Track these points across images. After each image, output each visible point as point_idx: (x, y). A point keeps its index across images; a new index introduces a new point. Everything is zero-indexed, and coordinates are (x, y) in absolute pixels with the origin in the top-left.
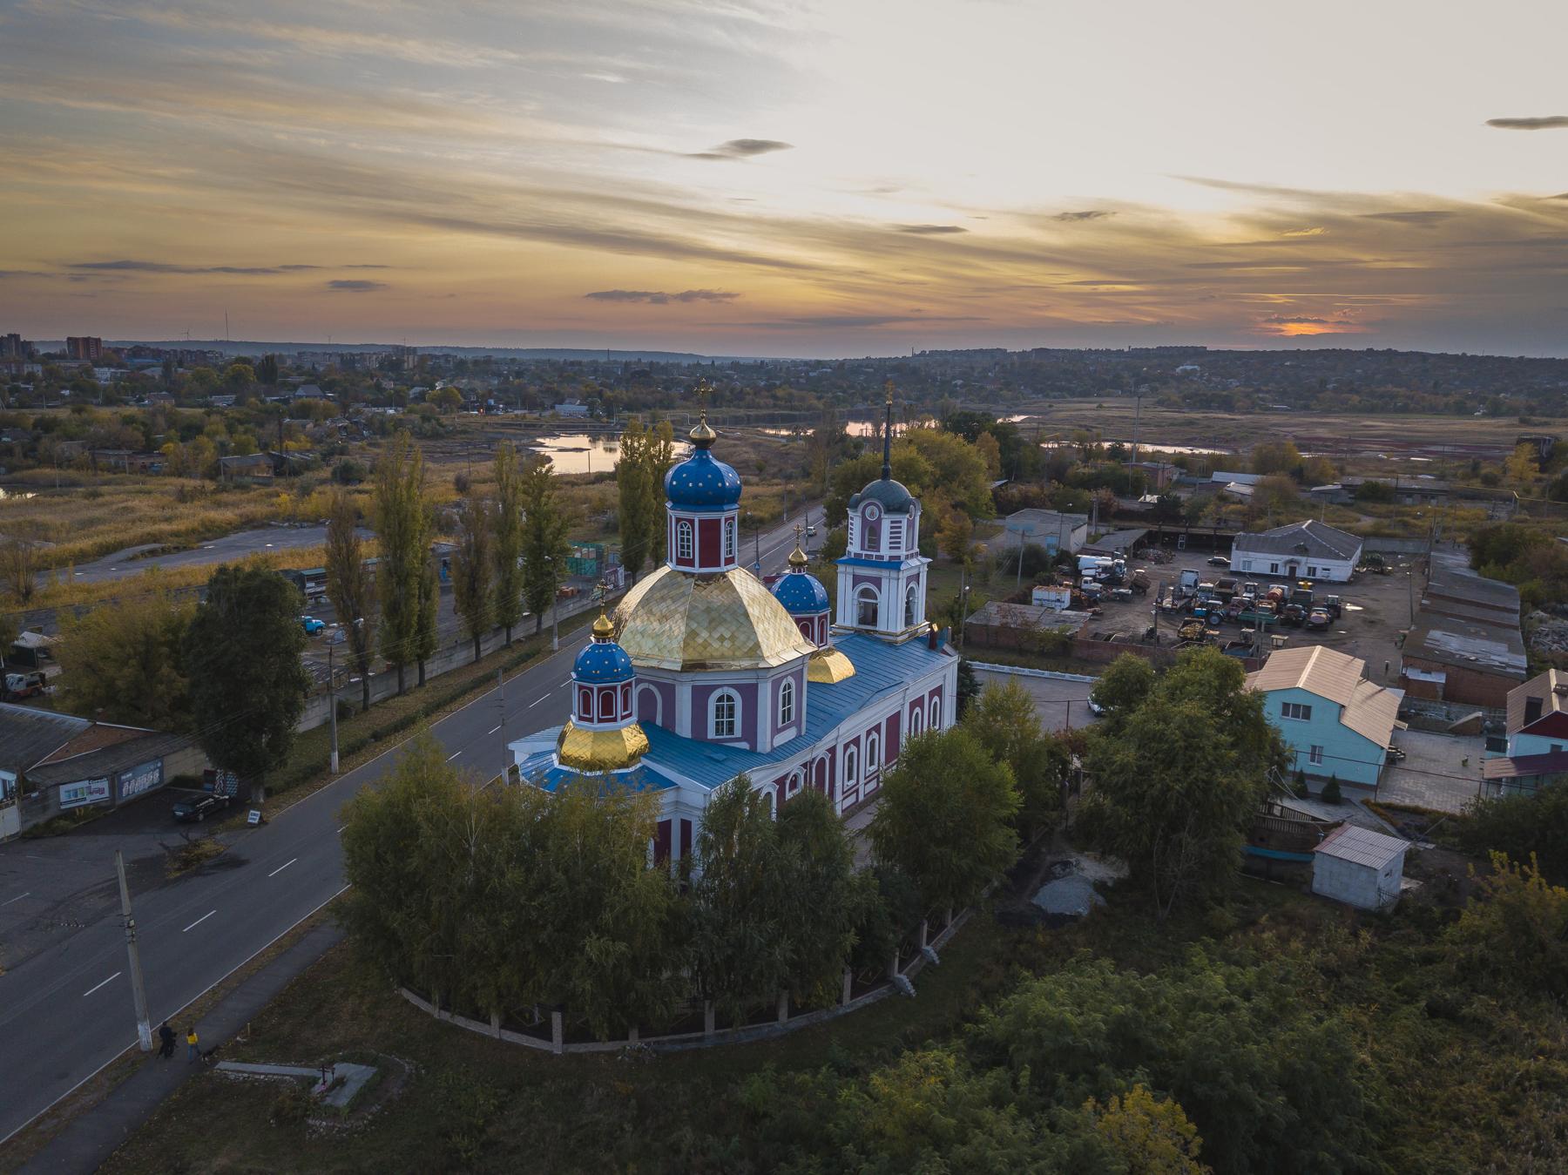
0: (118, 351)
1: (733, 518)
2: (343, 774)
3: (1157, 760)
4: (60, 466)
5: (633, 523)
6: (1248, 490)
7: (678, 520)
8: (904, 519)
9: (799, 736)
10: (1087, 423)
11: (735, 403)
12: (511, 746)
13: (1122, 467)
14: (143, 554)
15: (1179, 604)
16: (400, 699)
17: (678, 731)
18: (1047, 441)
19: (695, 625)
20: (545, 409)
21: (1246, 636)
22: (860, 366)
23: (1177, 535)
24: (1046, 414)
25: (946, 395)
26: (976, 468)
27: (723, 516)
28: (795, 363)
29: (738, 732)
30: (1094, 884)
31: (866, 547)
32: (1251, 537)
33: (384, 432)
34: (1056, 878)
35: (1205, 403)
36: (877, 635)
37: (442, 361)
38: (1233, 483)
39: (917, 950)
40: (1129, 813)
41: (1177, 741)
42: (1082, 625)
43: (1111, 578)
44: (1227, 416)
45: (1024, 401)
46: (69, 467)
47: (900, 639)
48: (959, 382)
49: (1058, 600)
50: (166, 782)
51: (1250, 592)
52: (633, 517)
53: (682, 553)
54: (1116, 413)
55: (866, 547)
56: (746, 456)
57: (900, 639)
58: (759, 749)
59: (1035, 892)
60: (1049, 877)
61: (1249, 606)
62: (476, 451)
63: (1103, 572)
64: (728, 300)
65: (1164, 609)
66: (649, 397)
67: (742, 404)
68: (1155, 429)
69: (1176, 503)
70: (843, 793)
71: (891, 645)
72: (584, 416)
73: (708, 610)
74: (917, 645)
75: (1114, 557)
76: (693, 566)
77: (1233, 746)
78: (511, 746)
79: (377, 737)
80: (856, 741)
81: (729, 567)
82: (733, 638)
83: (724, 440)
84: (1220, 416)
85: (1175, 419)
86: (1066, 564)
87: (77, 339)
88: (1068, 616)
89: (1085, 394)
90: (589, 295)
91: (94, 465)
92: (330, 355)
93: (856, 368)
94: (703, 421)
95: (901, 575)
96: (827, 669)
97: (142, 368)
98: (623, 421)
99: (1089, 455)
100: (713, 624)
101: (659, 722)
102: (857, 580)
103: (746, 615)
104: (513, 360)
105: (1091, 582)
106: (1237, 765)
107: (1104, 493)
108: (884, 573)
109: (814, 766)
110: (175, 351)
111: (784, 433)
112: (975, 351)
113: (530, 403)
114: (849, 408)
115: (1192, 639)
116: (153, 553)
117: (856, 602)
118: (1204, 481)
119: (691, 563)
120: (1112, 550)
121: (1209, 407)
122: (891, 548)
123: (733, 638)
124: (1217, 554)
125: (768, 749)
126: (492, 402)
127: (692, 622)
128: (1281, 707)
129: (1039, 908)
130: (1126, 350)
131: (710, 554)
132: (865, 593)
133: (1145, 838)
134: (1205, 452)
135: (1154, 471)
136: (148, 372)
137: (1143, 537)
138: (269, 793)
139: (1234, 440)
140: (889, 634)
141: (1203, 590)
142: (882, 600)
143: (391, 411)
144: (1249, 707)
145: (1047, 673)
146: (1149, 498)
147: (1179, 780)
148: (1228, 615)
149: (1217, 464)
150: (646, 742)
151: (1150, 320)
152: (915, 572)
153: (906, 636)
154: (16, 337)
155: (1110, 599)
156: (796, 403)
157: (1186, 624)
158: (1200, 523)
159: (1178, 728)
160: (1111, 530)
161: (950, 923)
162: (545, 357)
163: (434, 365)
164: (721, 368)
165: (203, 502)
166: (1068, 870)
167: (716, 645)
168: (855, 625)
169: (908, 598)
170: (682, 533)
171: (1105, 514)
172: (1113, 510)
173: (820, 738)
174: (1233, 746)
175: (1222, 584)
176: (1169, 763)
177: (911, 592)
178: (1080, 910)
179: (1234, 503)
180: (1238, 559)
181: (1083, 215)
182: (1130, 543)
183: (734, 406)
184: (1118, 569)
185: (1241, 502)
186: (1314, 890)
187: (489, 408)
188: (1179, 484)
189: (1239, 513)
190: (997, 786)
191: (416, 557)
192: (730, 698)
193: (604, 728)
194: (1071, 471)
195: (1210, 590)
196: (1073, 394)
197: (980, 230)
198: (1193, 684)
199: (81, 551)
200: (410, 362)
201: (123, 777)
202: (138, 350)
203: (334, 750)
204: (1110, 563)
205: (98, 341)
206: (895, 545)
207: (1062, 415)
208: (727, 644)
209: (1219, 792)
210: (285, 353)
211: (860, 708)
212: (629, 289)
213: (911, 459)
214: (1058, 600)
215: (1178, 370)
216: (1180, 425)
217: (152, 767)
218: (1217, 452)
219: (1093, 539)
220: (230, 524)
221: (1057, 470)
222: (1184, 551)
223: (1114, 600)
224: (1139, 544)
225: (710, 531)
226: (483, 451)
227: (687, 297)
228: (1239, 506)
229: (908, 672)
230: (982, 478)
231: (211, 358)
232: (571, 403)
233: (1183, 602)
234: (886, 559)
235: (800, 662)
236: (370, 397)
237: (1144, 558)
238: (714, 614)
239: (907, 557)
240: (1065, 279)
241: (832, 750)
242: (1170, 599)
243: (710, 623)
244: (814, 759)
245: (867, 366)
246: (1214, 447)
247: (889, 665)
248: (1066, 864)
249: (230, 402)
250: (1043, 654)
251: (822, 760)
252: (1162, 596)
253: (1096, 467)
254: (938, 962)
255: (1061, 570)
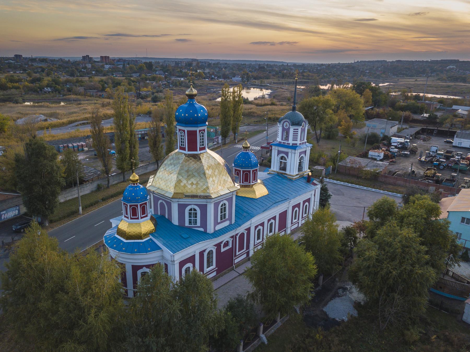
0: (114, 60)
1: (204, 130)
2: (83, 214)
3: (387, 255)
4: (76, 95)
5: (225, 120)
6: (466, 113)
7: (180, 130)
8: (300, 129)
9: (231, 224)
10: (409, 86)
11: (290, 77)
12: (111, 221)
13: (417, 103)
14: (81, 124)
15: (428, 159)
16: (123, 183)
17: (173, 222)
18: (392, 92)
19: (181, 177)
20: (229, 79)
21: (453, 177)
22: (335, 66)
23: (434, 130)
24: (396, 82)
25: (362, 76)
26: (359, 102)
27: (198, 129)
28: (315, 65)
29: (199, 224)
30: (355, 303)
31: (284, 139)
32: (463, 133)
33: (176, 86)
34: (339, 297)
35: (456, 79)
36: (286, 175)
37: (204, 63)
38: (460, 110)
39: (257, 336)
40: (370, 280)
41: (398, 249)
42: (384, 168)
43: (403, 147)
44: (464, 84)
45: (390, 78)
46: (79, 95)
47: (294, 177)
48: (368, 71)
49: (378, 156)
50: (21, 214)
51: (459, 156)
52: (225, 118)
53: (182, 145)
54: (421, 83)
55: (284, 139)
56: (287, 95)
57: (294, 177)
58: (208, 231)
59: (326, 304)
60: (336, 295)
61: (457, 163)
62: (202, 92)
63: (400, 144)
64: (294, 44)
65: (421, 161)
66: (262, 75)
67: (292, 77)
68: (435, 89)
69: (436, 117)
70: (254, 245)
71: (291, 180)
72: (241, 81)
73: (187, 171)
74: (303, 180)
75: (406, 138)
76: (185, 150)
77: (427, 253)
78: (111, 221)
79: (104, 200)
80: (262, 224)
81: (202, 152)
82: (197, 183)
83: (281, 90)
84: (460, 84)
85: (443, 85)
86: (387, 140)
87: (103, 57)
88: (379, 164)
89: (412, 76)
90: (251, 43)
91: (85, 95)
92: (173, 61)
93: (334, 66)
94: (191, 86)
95: (296, 152)
96: (254, 192)
97: (118, 65)
98: (251, 83)
99: (407, 98)
100: (189, 177)
101: (175, 221)
102: (279, 152)
103: (204, 174)
104: (226, 63)
105: (394, 148)
106: (427, 263)
107: (407, 113)
108: (289, 150)
109: (238, 237)
110: (129, 60)
111: (302, 87)
112: (376, 61)
113: (225, 77)
114: (328, 80)
115: (429, 176)
116: (84, 124)
117: (278, 161)
118: (449, 108)
119: (184, 149)
120: (405, 135)
121: (457, 81)
122: (293, 140)
123: (197, 183)
124: (449, 138)
125: (212, 231)
126: (213, 76)
127: (180, 176)
128: (461, 219)
129: (325, 314)
130: (429, 61)
131: (192, 145)
132: (282, 158)
133: (376, 293)
134: (452, 97)
135: (429, 105)
136: (119, 66)
137: (420, 130)
138: (51, 222)
139: (464, 93)
140: (290, 175)
141: (439, 154)
142: (288, 161)
143: (182, 79)
144: (441, 228)
145: (365, 188)
146: (425, 115)
147: (396, 269)
148: (448, 165)
149: (455, 102)
150: (154, 228)
151: (439, 50)
152: (304, 150)
153: (298, 176)
154: (88, 56)
155: (400, 156)
156: (310, 78)
157: (428, 169)
158: (444, 126)
159: (400, 242)
160: (408, 127)
161: (279, 320)
162: (236, 62)
163: (202, 64)
164: (290, 66)
165: (109, 107)
166: (345, 293)
167: (189, 187)
168: (278, 171)
169: (300, 160)
170: (181, 136)
171: (407, 120)
172: (411, 119)
173: (240, 226)
174: (427, 253)
175: (448, 152)
176: (393, 259)
177: (301, 159)
178: (344, 318)
179: (459, 117)
180: (456, 141)
181: (418, 14)
182: (414, 133)
183: (289, 78)
184: (406, 143)
185: (462, 117)
186: (463, 320)
187: (212, 78)
188: (439, 110)
189: (461, 121)
190: (304, 265)
191: (128, 134)
192: (195, 210)
193: (133, 222)
194: (397, 104)
195: (442, 155)
196: (407, 75)
197: (382, 19)
198: (413, 216)
199: (63, 122)
200: (194, 64)
201: (2, 213)
202: (120, 60)
203: (80, 206)
204: (403, 141)
205: (108, 57)
206: (295, 139)
207: (402, 83)
208: (194, 186)
209: (416, 277)
210: (160, 61)
211: (263, 211)
212: (263, 41)
213: (328, 100)
214: (378, 156)
215: (447, 68)
216: (445, 87)
217: (15, 209)
218: (456, 98)
219: (400, 130)
220: (112, 115)
221: (393, 104)
222: (436, 136)
223: (402, 156)
224: (418, 133)
225: (192, 136)
226: (204, 92)
227: (282, 43)
228: (461, 119)
229: (293, 193)
230: (361, 106)
231: (139, 62)
232: (237, 77)
233: (430, 159)
234: (291, 145)
235: (231, 194)
236: (177, 74)
237: (419, 138)
238: (190, 173)
239: (300, 144)
240: (411, 36)
241: (248, 230)
242: (424, 157)
243: (188, 176)
244: (237, 235)
245: (338, 66)
246: (455, 96)
247: (286, 190)
248: (345, 289)
249: (138, 76)
250: (365, 179)
251: (243, 234)
252: (421, 156)
253: (407, 103)
254: (266, 343)
255: (383, 143)
